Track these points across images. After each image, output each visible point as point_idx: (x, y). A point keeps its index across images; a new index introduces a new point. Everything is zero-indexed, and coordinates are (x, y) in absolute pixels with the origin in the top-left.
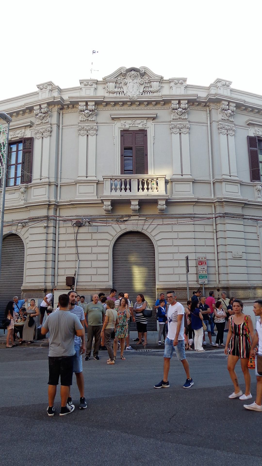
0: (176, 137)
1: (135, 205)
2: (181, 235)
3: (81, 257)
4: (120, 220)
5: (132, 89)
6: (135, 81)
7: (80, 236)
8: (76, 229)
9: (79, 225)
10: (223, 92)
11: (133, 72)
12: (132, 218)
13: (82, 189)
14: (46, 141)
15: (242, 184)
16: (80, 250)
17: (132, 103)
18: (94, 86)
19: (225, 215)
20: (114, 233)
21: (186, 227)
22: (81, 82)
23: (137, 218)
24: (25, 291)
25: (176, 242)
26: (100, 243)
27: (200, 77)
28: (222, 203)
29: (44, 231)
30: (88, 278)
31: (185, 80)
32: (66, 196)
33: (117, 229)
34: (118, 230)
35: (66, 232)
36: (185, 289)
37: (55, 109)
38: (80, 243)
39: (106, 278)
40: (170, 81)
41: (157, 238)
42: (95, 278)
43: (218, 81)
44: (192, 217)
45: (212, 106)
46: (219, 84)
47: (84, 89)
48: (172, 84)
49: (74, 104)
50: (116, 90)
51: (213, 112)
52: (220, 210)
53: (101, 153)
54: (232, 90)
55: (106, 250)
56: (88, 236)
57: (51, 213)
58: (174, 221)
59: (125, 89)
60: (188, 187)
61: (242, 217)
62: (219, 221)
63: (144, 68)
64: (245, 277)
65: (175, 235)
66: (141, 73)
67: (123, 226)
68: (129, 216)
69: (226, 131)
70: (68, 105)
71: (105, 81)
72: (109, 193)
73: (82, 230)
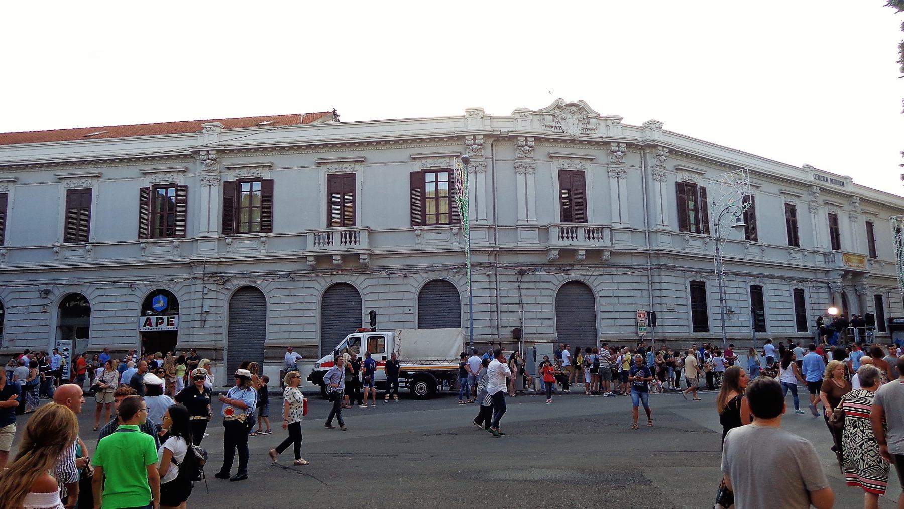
0: (614, 182)
1: (581, 255)
2: (622, 286)
3: (526, 307)
4: (562, 269)
5: (573, 128)
6: (575, 117)
7: (523, 286)
8: (520, 277)
9: (522, 273)
10: (657, 137)
11: (574, 108)
12: (575, 267)
13: (522, 234)
14: (481, 177)
15: (672, 234)
16: (525, 300)
17: (573, 141)
18: (531, 117)
19: (660, 267)
20: (557, 283)
21: (625, 278)
22: (468, 111)
23: (580, 267)
24: (267, 348)
25: (617, 293)
26: (545, 293)
27: (634, 116)
28: (658, 254)
29: (487, 279)
30: (533, 330)
31: (621, 118)
32: (505, 242)
33: (559, 279)
34: (420, 280)
35: (508, 282)
36: (722, 339)
37: (491, 141)
38: (524, 293)
39: (313, 335)
40: (606, 119)
41: (599, 288)
42: (540, 330)
43: (653, 122)
44: (631, 268)
45: (648, 150)
46: (653, 126)
47: (519, 120)
48: (609, 122)
49: (511, 138)
50: (554, 124)
51: (649, 156)
52: (655, 262)
53: (535, 198)
54: (665, 132)
55: (549, 300)
56: (531, 286)
57: (492, 260)
58: (614, 272)
59: (563, 124)
60: (627, 236)
61: (672, 268)
62: (655, 272)
63: (582, 101)
64: (617, 330)
65: (614, 286)
66: (578, 108)
67: (566, 276)
68: (572, 265)
69: (523, 170)
70: (504, 138)
71: (541, 113)
72: (311, 247)
73: (525, 278)
